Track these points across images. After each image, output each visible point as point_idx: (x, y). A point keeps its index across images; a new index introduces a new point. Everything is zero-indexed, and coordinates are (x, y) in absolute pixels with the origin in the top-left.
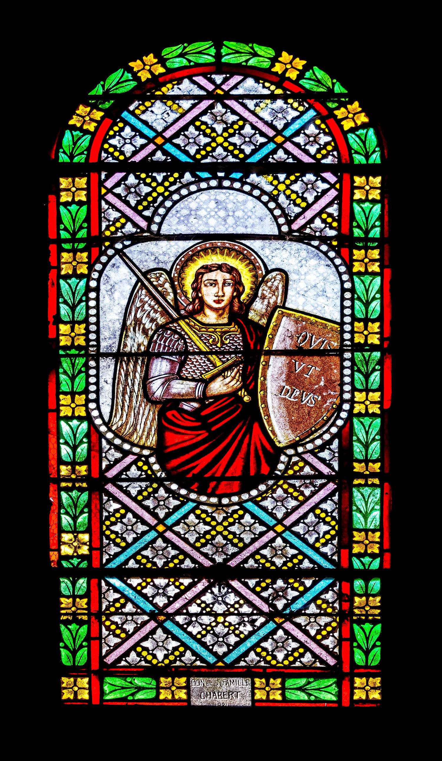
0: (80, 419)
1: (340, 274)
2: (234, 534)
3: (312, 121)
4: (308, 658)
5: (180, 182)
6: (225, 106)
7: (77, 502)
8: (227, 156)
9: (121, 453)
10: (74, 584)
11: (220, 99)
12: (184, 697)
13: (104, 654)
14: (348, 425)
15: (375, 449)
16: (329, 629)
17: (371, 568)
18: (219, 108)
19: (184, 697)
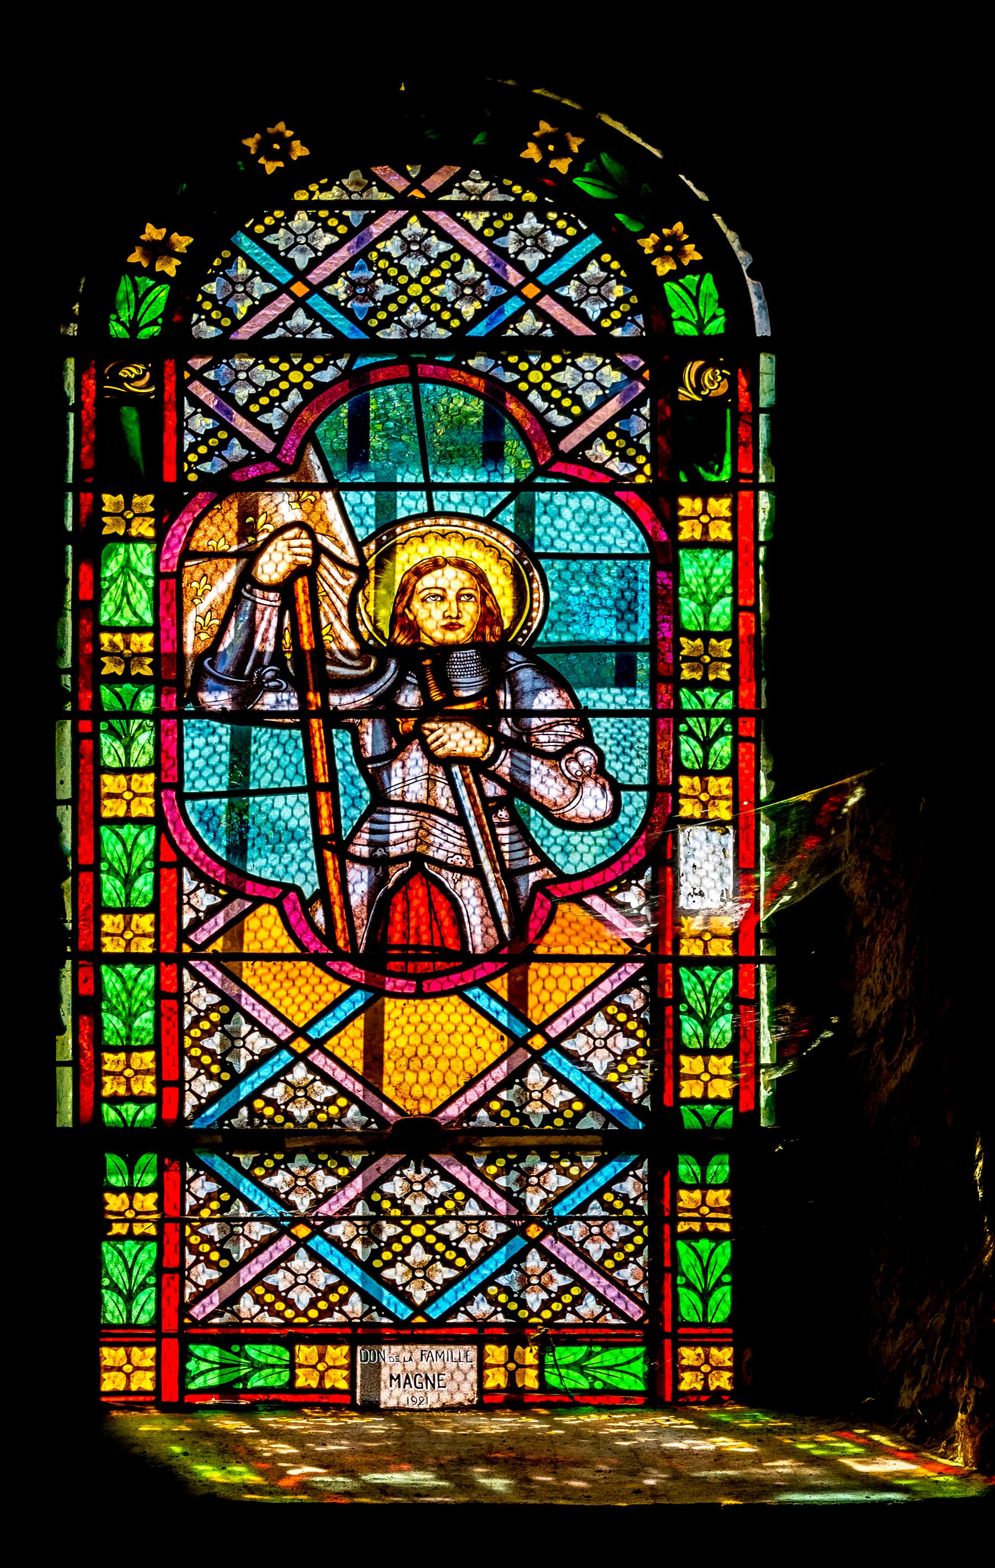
3: (595, 254)
4: (590, 1307)
6: (425, 222)
11: (415, 208)
12: (343, 1385)
13: (187, 1299)
15: (722, 614)
16: (630, 1248)
18: (414, 226)
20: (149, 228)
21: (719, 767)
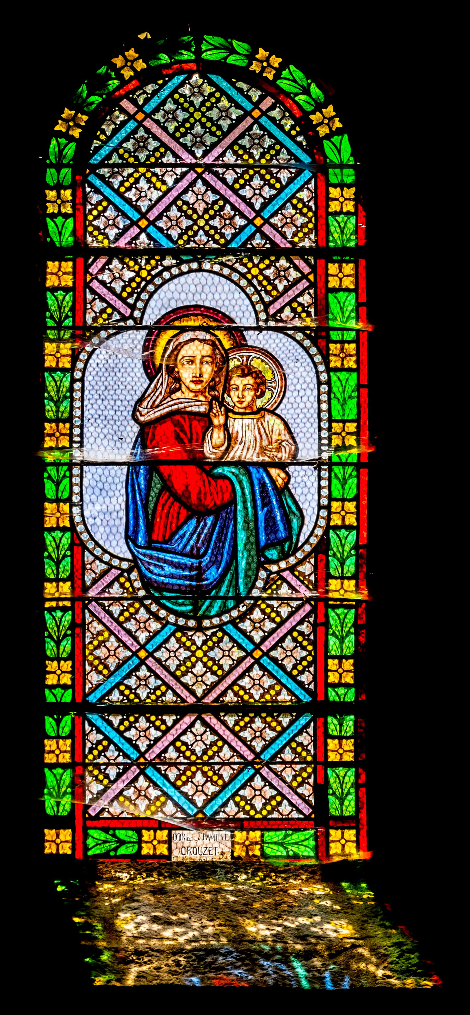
0: (64, 530)
1: (315, 365)
2: (215, 228)
5: (162, 265)
7: (60, 622)
8: (208, 241)
9: (105, 255)
10: (58, 722)
12: (166, 852)
14: (324, 352)
17: (346, 700)
19: (166, 852)
20: (66, 110)
21: (349, 575)
